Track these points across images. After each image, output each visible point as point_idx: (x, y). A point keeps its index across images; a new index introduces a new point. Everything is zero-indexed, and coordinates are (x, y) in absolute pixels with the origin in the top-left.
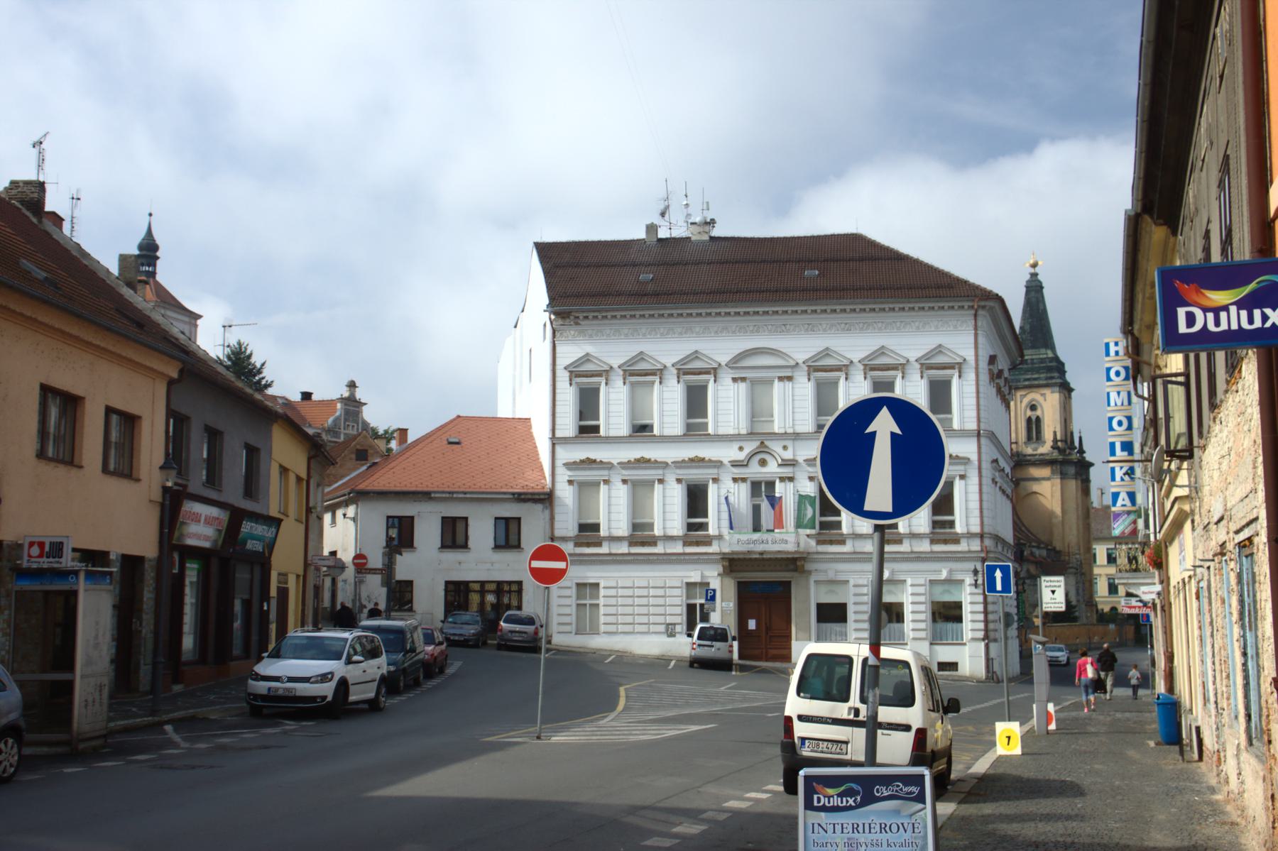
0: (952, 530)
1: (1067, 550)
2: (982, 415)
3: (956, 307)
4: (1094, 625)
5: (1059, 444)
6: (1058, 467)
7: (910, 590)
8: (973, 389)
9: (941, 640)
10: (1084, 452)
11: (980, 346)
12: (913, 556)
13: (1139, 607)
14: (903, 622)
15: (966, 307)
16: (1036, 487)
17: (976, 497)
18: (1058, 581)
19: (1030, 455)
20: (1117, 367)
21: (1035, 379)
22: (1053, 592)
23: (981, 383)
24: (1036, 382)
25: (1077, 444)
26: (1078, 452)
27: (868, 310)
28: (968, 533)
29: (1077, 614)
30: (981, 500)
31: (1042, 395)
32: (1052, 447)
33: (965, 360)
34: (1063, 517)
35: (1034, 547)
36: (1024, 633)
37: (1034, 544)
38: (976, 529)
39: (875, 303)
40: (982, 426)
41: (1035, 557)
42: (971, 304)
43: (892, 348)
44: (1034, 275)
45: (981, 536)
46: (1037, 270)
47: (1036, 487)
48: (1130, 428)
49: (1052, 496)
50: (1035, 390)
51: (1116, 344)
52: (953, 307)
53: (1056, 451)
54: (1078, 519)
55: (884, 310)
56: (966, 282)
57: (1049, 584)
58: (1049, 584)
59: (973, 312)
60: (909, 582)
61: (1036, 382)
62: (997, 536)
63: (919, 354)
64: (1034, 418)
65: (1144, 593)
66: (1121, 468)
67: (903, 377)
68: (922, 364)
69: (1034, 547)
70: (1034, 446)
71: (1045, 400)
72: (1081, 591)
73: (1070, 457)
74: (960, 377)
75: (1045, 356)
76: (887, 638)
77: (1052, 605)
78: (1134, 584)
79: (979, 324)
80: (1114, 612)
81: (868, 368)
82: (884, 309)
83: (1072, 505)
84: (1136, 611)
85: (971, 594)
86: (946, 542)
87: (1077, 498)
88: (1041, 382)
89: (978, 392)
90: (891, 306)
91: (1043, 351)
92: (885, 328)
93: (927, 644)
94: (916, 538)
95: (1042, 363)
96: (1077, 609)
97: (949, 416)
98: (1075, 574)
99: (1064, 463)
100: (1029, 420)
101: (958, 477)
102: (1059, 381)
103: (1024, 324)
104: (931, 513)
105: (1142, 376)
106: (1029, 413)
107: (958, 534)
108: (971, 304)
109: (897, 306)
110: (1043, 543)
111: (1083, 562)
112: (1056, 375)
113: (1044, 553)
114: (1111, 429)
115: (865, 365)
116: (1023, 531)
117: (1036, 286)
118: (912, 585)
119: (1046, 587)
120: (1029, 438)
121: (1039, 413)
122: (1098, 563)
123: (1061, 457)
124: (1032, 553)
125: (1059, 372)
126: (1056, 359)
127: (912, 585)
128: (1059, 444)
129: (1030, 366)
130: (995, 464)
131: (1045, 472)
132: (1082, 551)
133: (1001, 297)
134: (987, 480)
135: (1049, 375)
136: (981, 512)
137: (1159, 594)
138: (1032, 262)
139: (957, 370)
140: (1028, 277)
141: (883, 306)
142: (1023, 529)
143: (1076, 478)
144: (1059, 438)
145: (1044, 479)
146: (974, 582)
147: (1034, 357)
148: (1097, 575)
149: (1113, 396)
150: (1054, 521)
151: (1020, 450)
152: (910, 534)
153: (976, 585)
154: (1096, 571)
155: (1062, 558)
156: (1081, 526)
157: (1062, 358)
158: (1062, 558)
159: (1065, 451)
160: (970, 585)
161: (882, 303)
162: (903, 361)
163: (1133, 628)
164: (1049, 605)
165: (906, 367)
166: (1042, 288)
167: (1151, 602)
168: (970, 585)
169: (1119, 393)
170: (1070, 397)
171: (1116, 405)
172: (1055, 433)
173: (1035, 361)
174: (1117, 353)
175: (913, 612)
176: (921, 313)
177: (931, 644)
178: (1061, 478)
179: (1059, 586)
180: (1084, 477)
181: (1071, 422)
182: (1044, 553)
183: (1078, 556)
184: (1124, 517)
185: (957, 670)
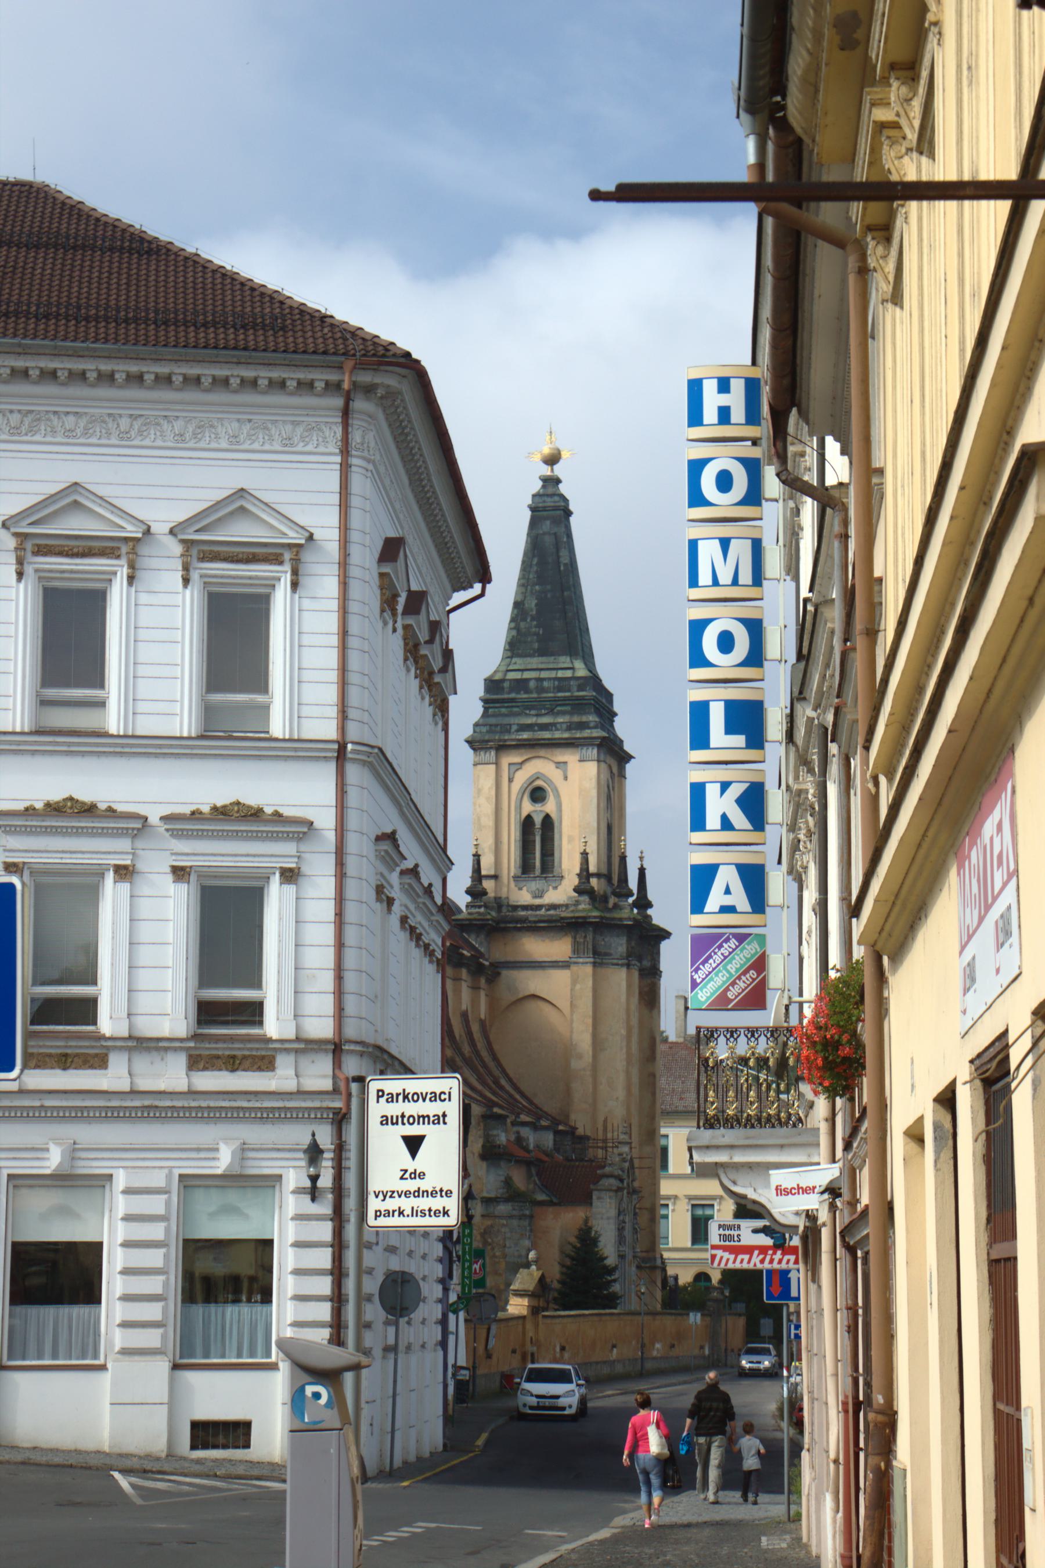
0: (254, 1031)
1: (601, 1136)
2: (354, 696)
3: (292, 384)
4: (654, 1314)
5: (594, 882)
6: (590, 937)
7: (121, 1205)
8: (332, 623)
9: (207, 1355)
10: (649, 905)
11: (355, 501)
12: (137, 1103)
13: (763, 1250)
14: (99, 1302)
15: (320, 385)
16: (533, 982)
17: (327, 934)
18: (435, 1097)
19: (525, 908)
20: (723, 459)
21: (544, 727)
22: (413, 1144)
23: (353, 607)
24: (547, 735)
25: (633, 884)
26: (635, 904)
27: (34, 373)
28: (298, 1039)
29: (616, 1288)
30: (340, 945)
31: (558, 764)
32: (576, 890)
33: (311, 537)
34: (595, 1057)
35: (524, 1124)
36: (483, 1333)
37: (524, 1118)
38: (322, 1028)
39: (56, 355)
40: (354, 732)
41: (526, 1149)
42: (333, 377)
43: (101, 491)
44: (551, 482)
45: (337, 1048)
46: (559, 470)
47: (533, 982)
48: (755, 657)
49: (573, 1006)
50: (542, 752)
51: (724, 385)
52: (282, 384)
53: (585, 898)
54: (629, 1061)
55: (81, 376)
56: (324, 319)
57: (395, 1109)
58: (395, 1109)
59: (339, 402)
60: (121, 1180)
61: (547, 735)
62: (379, 1048)
63: (181, 513)
64: (538, 820)
65: (780, 1191)
66: (725, 786)
67: (131, 579)
68: (188, 544)
69: (524, 1124)
70: (534, 885)
71: (566, 778)
72: (628, 1233)
73: (617, 915)
74: (295, 585)
75: (568, 674)
76: (199, 1349)
77: (406, 1204)
78: (750, 1166)
79: (356, 437)
80: (703, 1284)
81: (29, 546)
82: (83, 375)
83: (617, 1028)
84: (755, 1262)
85: (298, 1217)
86: (233, 1064)
87: (628, 1010)
88: (558, 735)
89: (344, 633)
90: (105, 367)
91: (564, 661)
92: (85, 433)
93: (162, 1366)
94: (148, 1049)
95: (560, 689)
96: (616, 1275)
97: (259, 698)
98: (619, 1190)
99: (604, 926)
100: (527, 823)
101: (277, 877)
102: (598, 733)
103: (524, 594)
104: (194, 981)
105: (803, 415)
106: (528, 807)
107: (270, 1040)
108: (333, 377)
109: (122, 368)
110: (546, 1115)
111: (636, 1163)
112: (592, 718)
113: (548, 1140)
114: (698, 659)
115: (21, 537)
116: (502, 1088)
117: (556, 508)
118: (128, 1191)
119: (385, 1121)
120: (526, 867)
121: (549, 807)
122: (671, 1170)
123: (596, 913)
124: (519, 1140)
125: (598, 713)
126: (594, 681)
127: (128, 1191)
128: (594, 882)
129: (535, 695)
130: (386, 846)
131: (559, 948)
132: (635, 1140)
133: (418, 362)
134: (360, 890)
135: (576, 719)
136: (339, 978)
137: (832, 1191)
138: (546, 450)
139: (287, 567)
140: (537, 486)
141: (78, 365)
142: (503, 1082)
143: (628, 966)
144: (593, 868)
145: (555, 965)
146: (308, 1184)
147: (544, 675)
148: (668, 1198)
149: (709, 551)
150: (575, 1064)
151: (504, 894)
152: (131, 1038)
153: (314, 1193)
154: (666, 1188)
155: (590, 1154)
156: (635, 1079)
157: (608, 682)
158: (590, 1154)
159: (605, 899)
160: (298, 1191)
161: (77, 355)
162: (133, 531)
163: (742, 1321)
164: (391, 1204)
165: (144, 550)
166: (568, 513)
167: (801, 1223)
168: (298, 1191)
169: (725, 544)
170: (622, 775)
171: (716, 582)
172: (585, 855)
173: (546, 684)
174: (724, 415)
175: (126, 1272)
176: (191, 395)
177: (176, 1367)
178: (595, 964)
179: (441, 1119)
180: (646, 963)
181: (622, 831)
182: (548, 1140)
183: (625, 1149)
184: (726, 949)
185: (247, 1445)
